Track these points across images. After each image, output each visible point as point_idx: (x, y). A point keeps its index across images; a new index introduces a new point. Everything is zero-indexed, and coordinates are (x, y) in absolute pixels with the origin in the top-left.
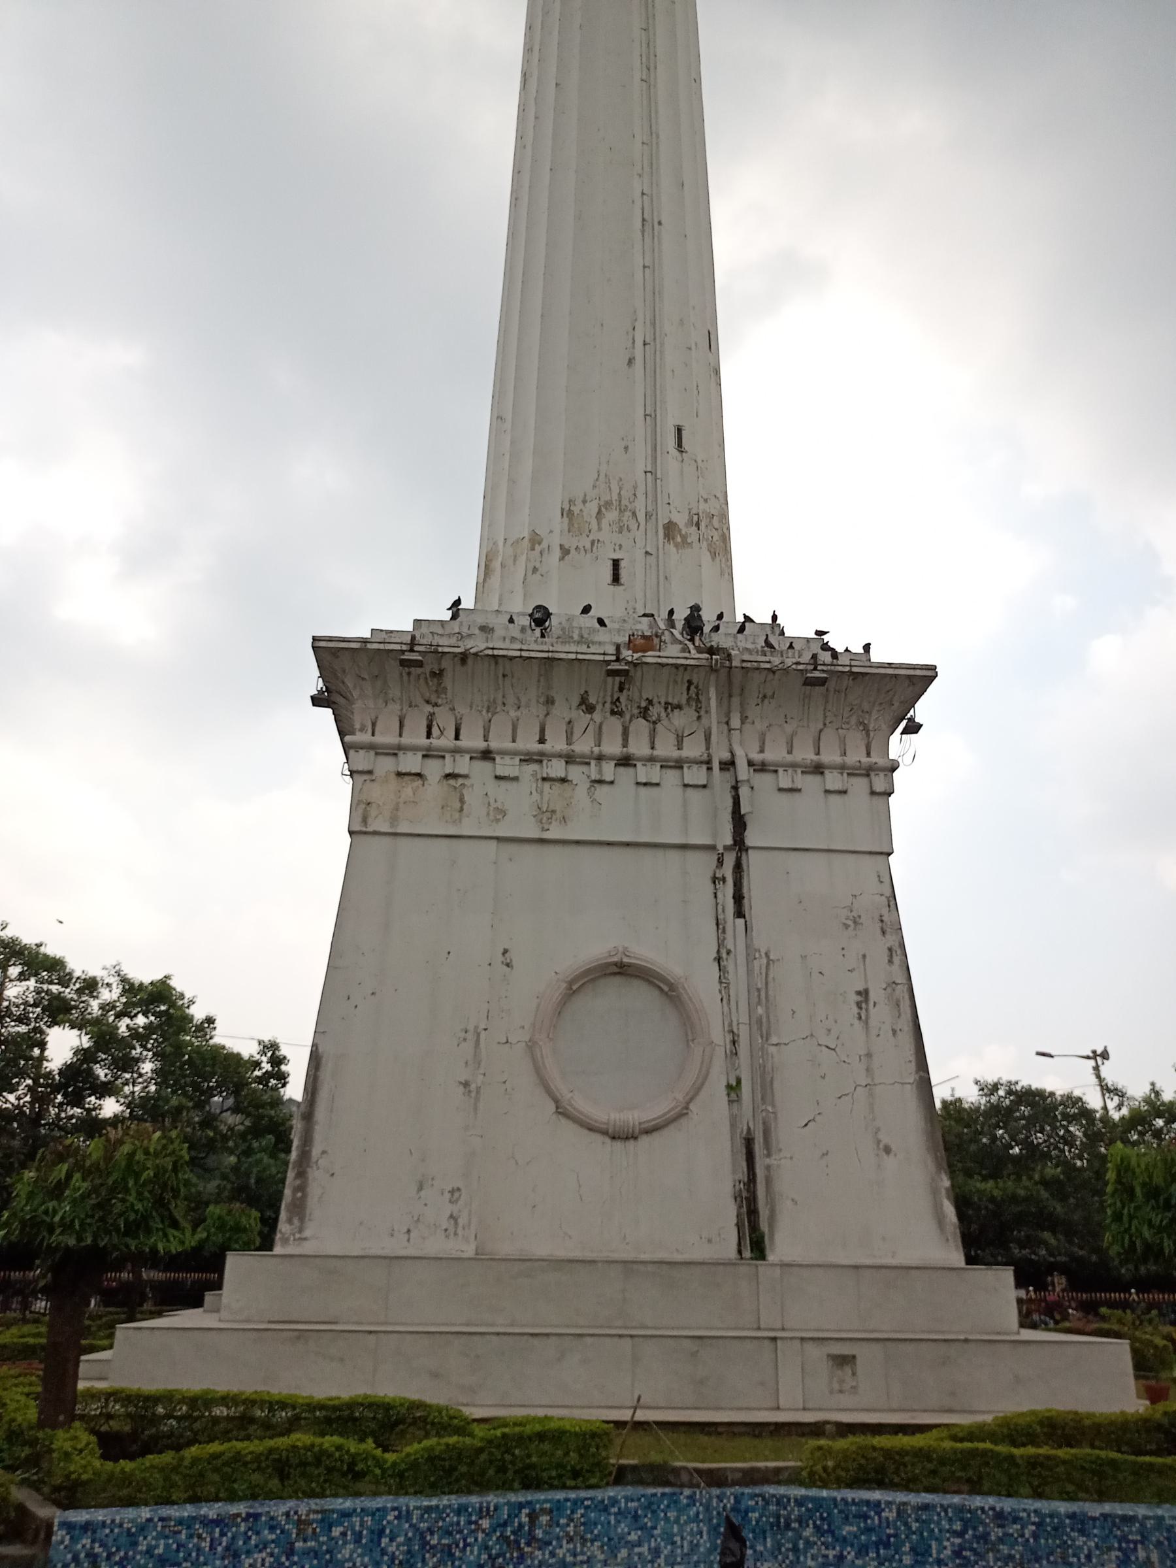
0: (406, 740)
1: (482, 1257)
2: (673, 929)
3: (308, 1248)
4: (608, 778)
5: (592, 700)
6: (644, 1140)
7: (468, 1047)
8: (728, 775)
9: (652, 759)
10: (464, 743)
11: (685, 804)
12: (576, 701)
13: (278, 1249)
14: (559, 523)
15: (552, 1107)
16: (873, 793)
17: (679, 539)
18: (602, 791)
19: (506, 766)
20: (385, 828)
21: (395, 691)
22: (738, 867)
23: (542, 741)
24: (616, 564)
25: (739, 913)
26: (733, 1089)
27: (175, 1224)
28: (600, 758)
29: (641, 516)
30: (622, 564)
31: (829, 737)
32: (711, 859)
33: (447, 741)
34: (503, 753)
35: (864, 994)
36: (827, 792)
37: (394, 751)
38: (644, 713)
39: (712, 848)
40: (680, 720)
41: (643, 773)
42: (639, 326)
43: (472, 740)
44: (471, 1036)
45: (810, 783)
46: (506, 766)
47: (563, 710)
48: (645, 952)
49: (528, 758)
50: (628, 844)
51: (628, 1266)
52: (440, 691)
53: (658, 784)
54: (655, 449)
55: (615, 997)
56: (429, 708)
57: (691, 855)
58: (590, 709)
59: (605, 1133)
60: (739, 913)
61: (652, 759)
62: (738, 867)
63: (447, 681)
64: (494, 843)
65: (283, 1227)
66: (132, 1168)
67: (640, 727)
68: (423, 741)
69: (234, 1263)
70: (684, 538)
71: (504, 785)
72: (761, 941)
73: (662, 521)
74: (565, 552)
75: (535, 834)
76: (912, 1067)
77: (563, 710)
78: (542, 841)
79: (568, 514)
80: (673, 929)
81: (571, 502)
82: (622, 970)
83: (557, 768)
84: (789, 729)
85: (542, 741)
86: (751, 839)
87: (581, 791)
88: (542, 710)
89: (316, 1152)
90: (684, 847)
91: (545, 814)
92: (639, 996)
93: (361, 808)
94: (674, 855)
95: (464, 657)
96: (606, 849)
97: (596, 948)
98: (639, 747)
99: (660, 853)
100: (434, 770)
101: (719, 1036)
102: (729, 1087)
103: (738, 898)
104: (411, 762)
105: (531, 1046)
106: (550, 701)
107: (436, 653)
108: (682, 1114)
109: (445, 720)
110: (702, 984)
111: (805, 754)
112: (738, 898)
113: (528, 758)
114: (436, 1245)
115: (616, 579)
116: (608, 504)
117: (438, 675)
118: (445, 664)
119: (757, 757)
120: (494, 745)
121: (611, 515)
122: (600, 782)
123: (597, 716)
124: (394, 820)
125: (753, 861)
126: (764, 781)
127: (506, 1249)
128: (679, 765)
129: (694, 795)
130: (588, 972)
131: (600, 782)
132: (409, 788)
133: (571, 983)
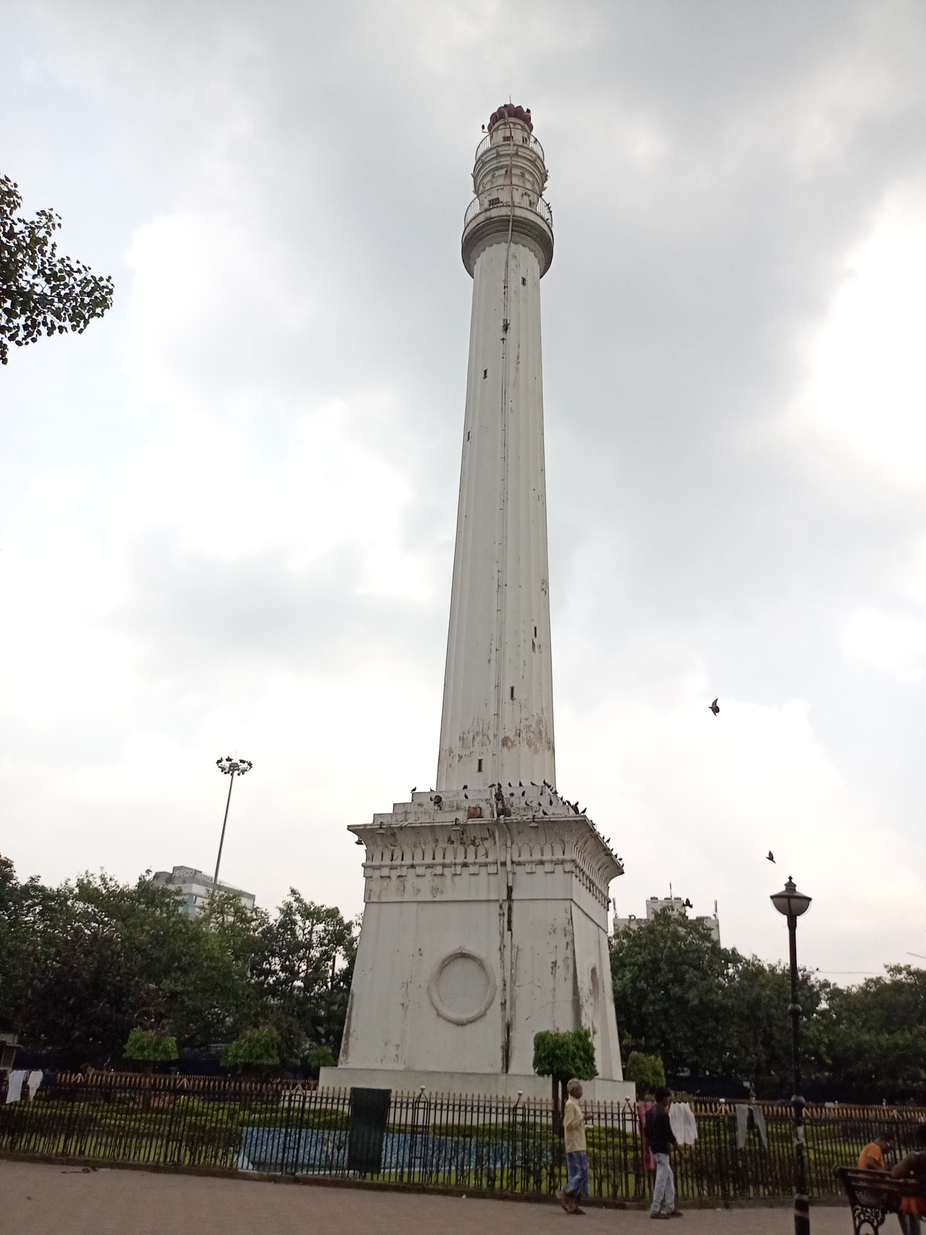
0: (383, 863)
1: (407, 1071)
2: (481, 935)
3: (349, 1066)
4: (459, 872)
5: (453, 839)
6: (469, 1025)
7: (404, 989)
8: (503, 868)
9: (475, 863)
10: (405, 862)
11: (488, 882)
12: (446, 840)
13: (339, 1066)
14: (458, 744)
15: (435, 1012)
16: (565, 872)
17: (510, 744)
18: (457, 879)
19: (420, 870)
20: (376, 900)
21: (379, 842)
22: (510, 909)
23: (434, 859)
24: (480, 761)
25: (510, 929)
26: (503, 1004)
27: (271, 1057)
28: (455, 864)
29: (491, 737)
30: (483, 762)
31: (547, 849)
32: (497, 905)
33: (397, 862)
34: (419, 865)
35: (555, 963)
36: (418, 876)
37: (379, 868)
38: (473, 843)
39: (498, 901)
40: (487, 844)
41: (472, 869)
42: (493, 643)
43: (408, 861)
44: (405, 985)
45: (539, 869)
46: (420, 870)
47: (442, 844)
48: (471, 949)
49: (429, 866)
50: (586, 915)
51: (452, 1074)
52: (396, 840)
53: (389, 877)
54: (498, 702)
55: (461, 966)
56: (392, 848)
57: (491, 904)
58: (452, 843)
59: (454, 1023)
60: (510, 929)
61: (475, 863)
62: (510, 909)
63: (398, 837)
64: (415, 906)
65: (341, 1058)
66: (258, 1041)
67: (471, 849)
68: (389, 863)
69: (323, 1071)
70: (512, 743)
71: (420, 878)
72: (515, 942)
73: (501, 737)
74: (460, 757)
75: (431, 899)
76: (571, 994)
77: (442, 844)
78: (434, 902)
79: (462, 739)
80: (481, 935)
81: (464, 733)
82: (463, 956)
83: (439, 870)
84: (531, 845)
85: (434, 859)
86: (515, 896)
87: (448, 880)
88: (434, 845)
89: (352, 1030)
90: (488, 901)
91: (435, 890)
92: (470, 966)
93: (368, 892)
94: (484, 905)
95: (401, 828)
96: (457, 905)
97: (452, 949)
98: (471, 859)
99: (480, 904)
100: (394, 874)
101: (499, 983)
102: (502, 1004)
103: (509, 922)
104: (385, 872)
105: (428, 988)
106: (436, 841)
107: (390, 827)
108: (482, 1016)
109: (398, 854)
110: (493, 961)
111: (537, 856)
112: (509, 922)
113: (429, 866)
114: (390, 1066)
115: (480, 769)
116: (478, 733)
117: (394, 835)
118: (395, 830)
119: (516, 859)
120: (415, 862)
121: (478, 739)
122: (455, 875)
123: (455, 845)
124: (380, 896)
125: (516, 906)
126: (518, 869)
127: (418, 1067)
128: (486, 865)
129: (493, 878)
130: (450, 957)
131: (455, 875)
132: (385, 883)
133: (444, 962)
